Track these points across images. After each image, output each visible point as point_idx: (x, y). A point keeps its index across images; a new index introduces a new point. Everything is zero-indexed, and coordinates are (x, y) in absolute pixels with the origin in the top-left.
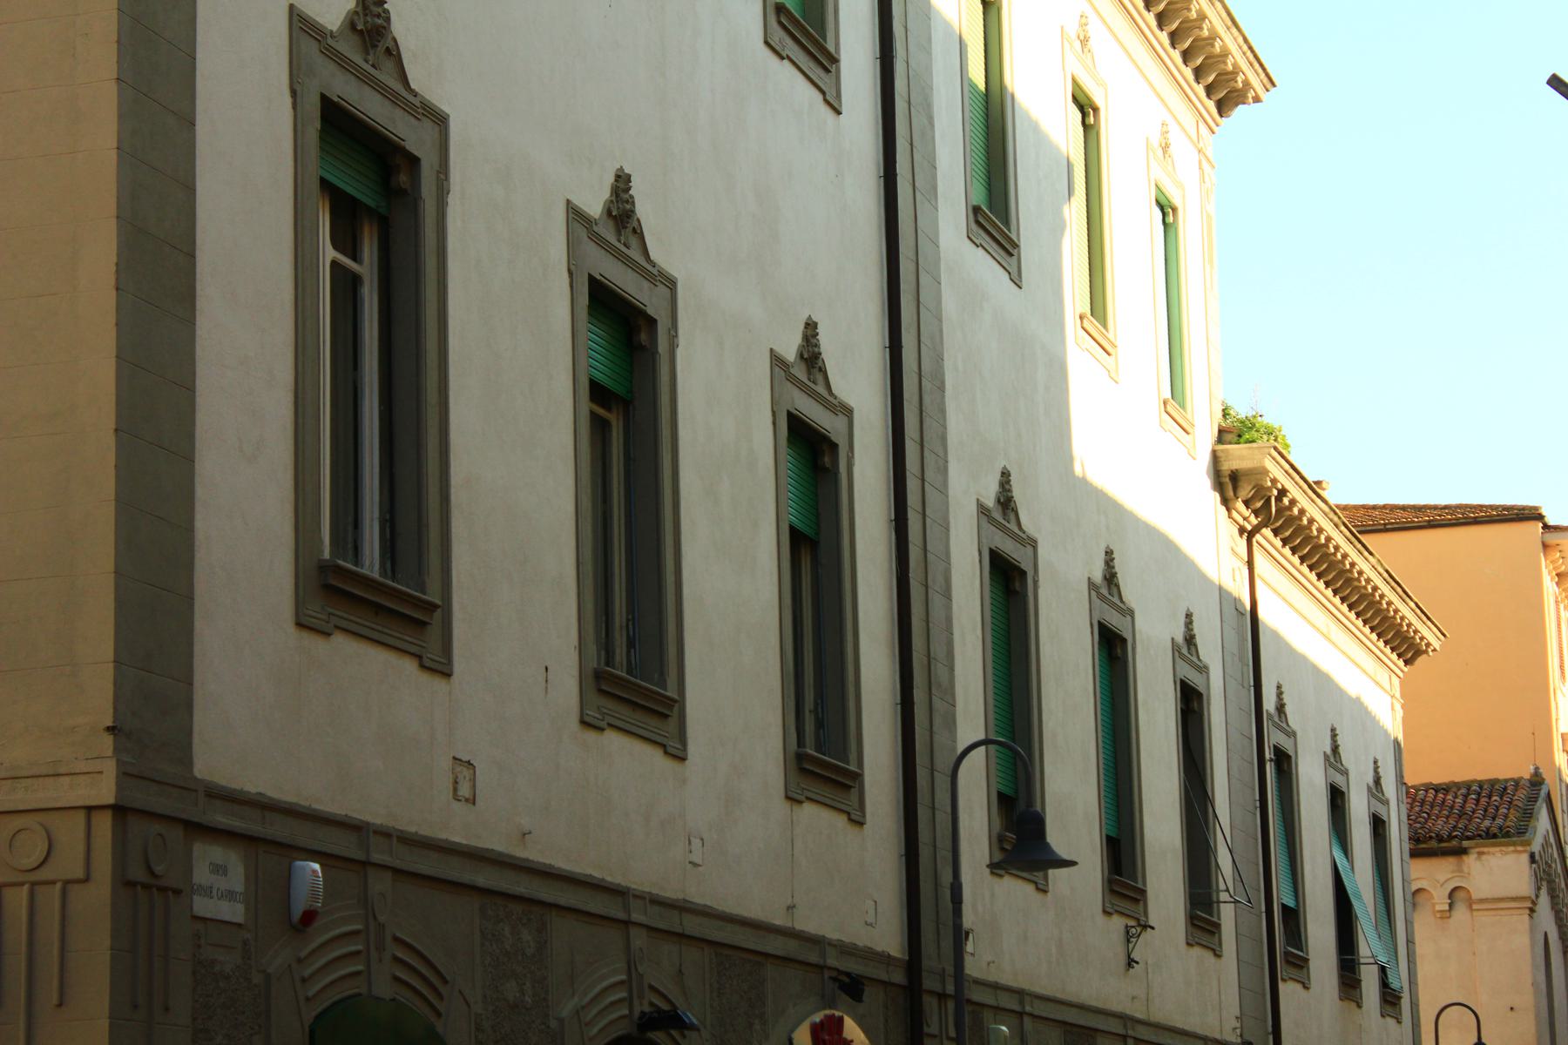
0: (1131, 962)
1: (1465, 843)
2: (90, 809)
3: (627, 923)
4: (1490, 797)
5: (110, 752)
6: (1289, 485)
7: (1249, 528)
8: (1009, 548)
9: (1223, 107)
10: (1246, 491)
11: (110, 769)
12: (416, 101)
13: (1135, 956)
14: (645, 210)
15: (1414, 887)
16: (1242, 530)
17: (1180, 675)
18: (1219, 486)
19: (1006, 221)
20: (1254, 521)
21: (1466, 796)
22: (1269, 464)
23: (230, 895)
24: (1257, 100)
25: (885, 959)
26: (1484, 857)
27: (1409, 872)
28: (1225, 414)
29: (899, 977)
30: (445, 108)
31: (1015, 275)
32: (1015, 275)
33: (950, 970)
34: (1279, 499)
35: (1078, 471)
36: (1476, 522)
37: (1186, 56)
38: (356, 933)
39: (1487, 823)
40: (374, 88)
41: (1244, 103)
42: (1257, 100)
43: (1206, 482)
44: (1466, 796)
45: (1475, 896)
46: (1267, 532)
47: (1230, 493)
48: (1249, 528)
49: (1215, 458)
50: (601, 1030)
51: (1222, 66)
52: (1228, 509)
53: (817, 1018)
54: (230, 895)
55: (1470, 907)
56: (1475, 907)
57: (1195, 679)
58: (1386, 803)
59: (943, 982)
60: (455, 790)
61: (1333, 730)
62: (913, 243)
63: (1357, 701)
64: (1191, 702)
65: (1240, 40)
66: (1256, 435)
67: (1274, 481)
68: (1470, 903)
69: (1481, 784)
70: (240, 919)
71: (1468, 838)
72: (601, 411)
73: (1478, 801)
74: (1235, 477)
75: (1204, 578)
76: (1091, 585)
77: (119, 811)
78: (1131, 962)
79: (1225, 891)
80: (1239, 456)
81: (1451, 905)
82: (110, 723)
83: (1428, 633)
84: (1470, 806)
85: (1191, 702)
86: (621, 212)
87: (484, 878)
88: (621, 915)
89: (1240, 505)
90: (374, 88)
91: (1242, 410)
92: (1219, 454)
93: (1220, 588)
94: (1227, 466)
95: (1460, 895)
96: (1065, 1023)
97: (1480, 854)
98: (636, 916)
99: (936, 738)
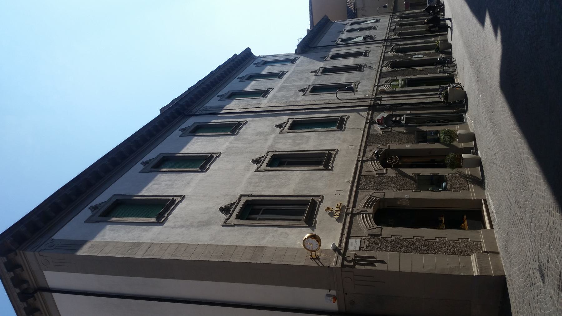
2: (342, 271)
8: (321, 71)
12: (238, 200)
14: (257, 157)
17: (287, 130)
19: (264, 91)
23: (356, 242)
30: (239, 195)
31: (272, 89)
32: (272, 89)
33: (370, 100)
37: (244, 61)
38: (362, 215)
50: (378, 166)
54: (356, 242)
57: (350, 23)
59: (372, 101)
61: (338, 32)
62: (266, 108)
64: (326, 71)
72: (286, 164)
79: (315, 252)
81: (364, 10)
86: (257, 161)
98: (361, 159)
99: (336, 102)
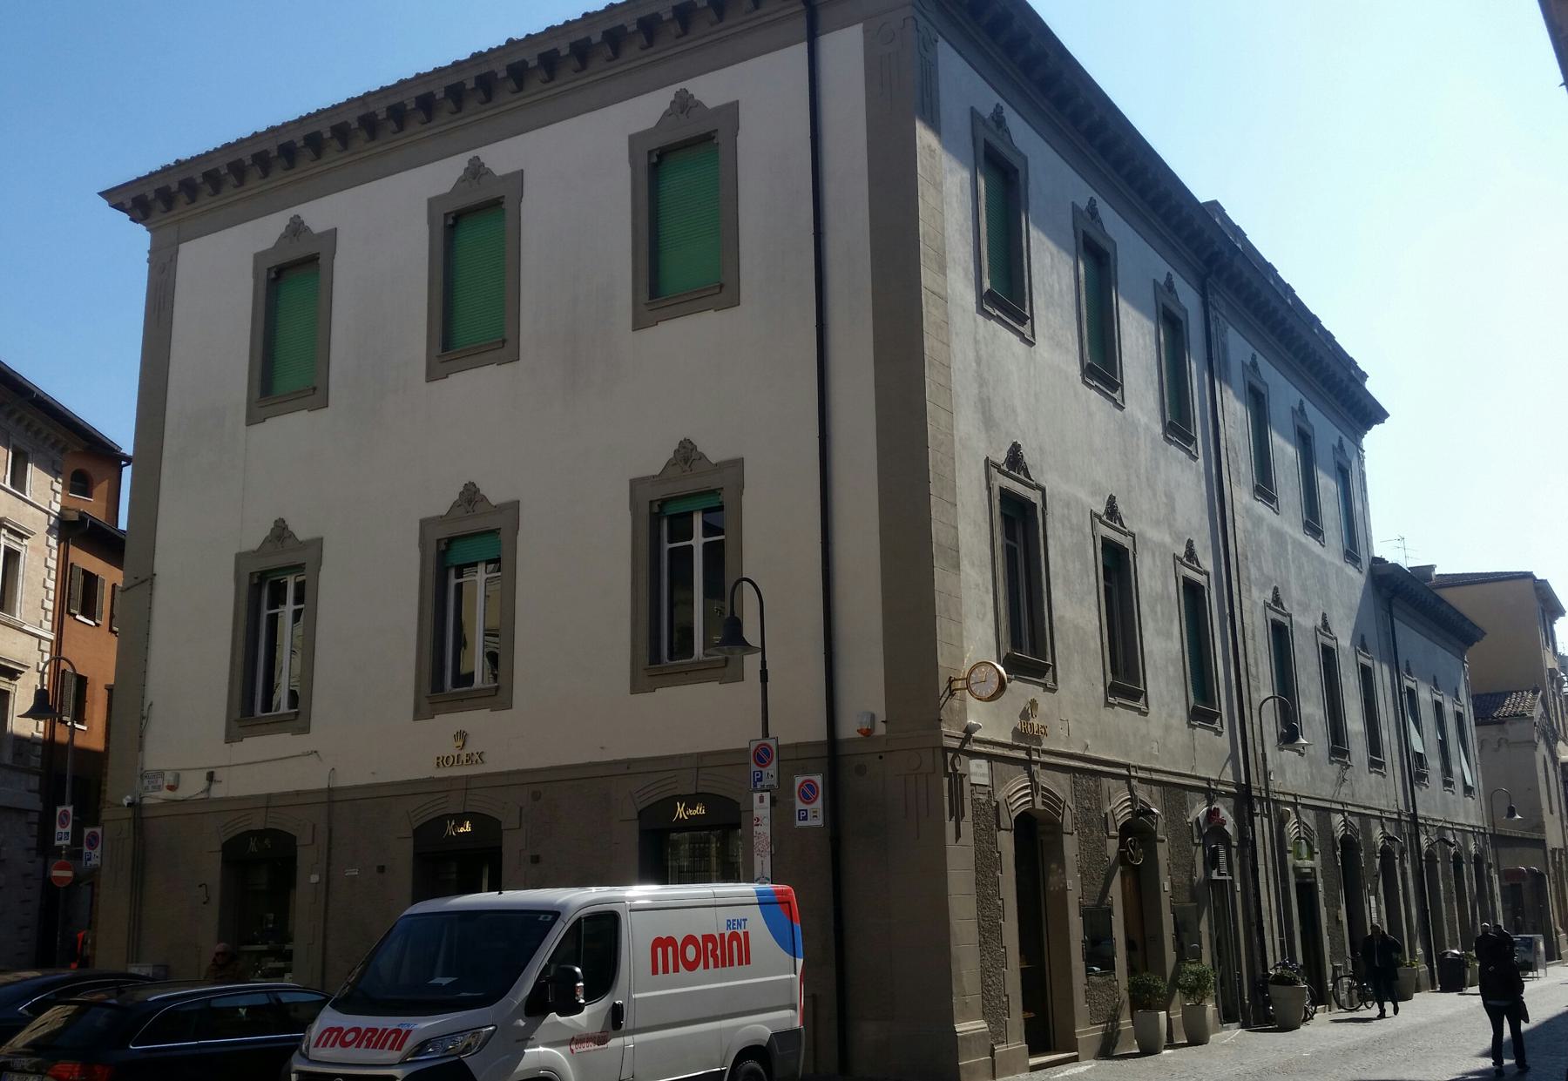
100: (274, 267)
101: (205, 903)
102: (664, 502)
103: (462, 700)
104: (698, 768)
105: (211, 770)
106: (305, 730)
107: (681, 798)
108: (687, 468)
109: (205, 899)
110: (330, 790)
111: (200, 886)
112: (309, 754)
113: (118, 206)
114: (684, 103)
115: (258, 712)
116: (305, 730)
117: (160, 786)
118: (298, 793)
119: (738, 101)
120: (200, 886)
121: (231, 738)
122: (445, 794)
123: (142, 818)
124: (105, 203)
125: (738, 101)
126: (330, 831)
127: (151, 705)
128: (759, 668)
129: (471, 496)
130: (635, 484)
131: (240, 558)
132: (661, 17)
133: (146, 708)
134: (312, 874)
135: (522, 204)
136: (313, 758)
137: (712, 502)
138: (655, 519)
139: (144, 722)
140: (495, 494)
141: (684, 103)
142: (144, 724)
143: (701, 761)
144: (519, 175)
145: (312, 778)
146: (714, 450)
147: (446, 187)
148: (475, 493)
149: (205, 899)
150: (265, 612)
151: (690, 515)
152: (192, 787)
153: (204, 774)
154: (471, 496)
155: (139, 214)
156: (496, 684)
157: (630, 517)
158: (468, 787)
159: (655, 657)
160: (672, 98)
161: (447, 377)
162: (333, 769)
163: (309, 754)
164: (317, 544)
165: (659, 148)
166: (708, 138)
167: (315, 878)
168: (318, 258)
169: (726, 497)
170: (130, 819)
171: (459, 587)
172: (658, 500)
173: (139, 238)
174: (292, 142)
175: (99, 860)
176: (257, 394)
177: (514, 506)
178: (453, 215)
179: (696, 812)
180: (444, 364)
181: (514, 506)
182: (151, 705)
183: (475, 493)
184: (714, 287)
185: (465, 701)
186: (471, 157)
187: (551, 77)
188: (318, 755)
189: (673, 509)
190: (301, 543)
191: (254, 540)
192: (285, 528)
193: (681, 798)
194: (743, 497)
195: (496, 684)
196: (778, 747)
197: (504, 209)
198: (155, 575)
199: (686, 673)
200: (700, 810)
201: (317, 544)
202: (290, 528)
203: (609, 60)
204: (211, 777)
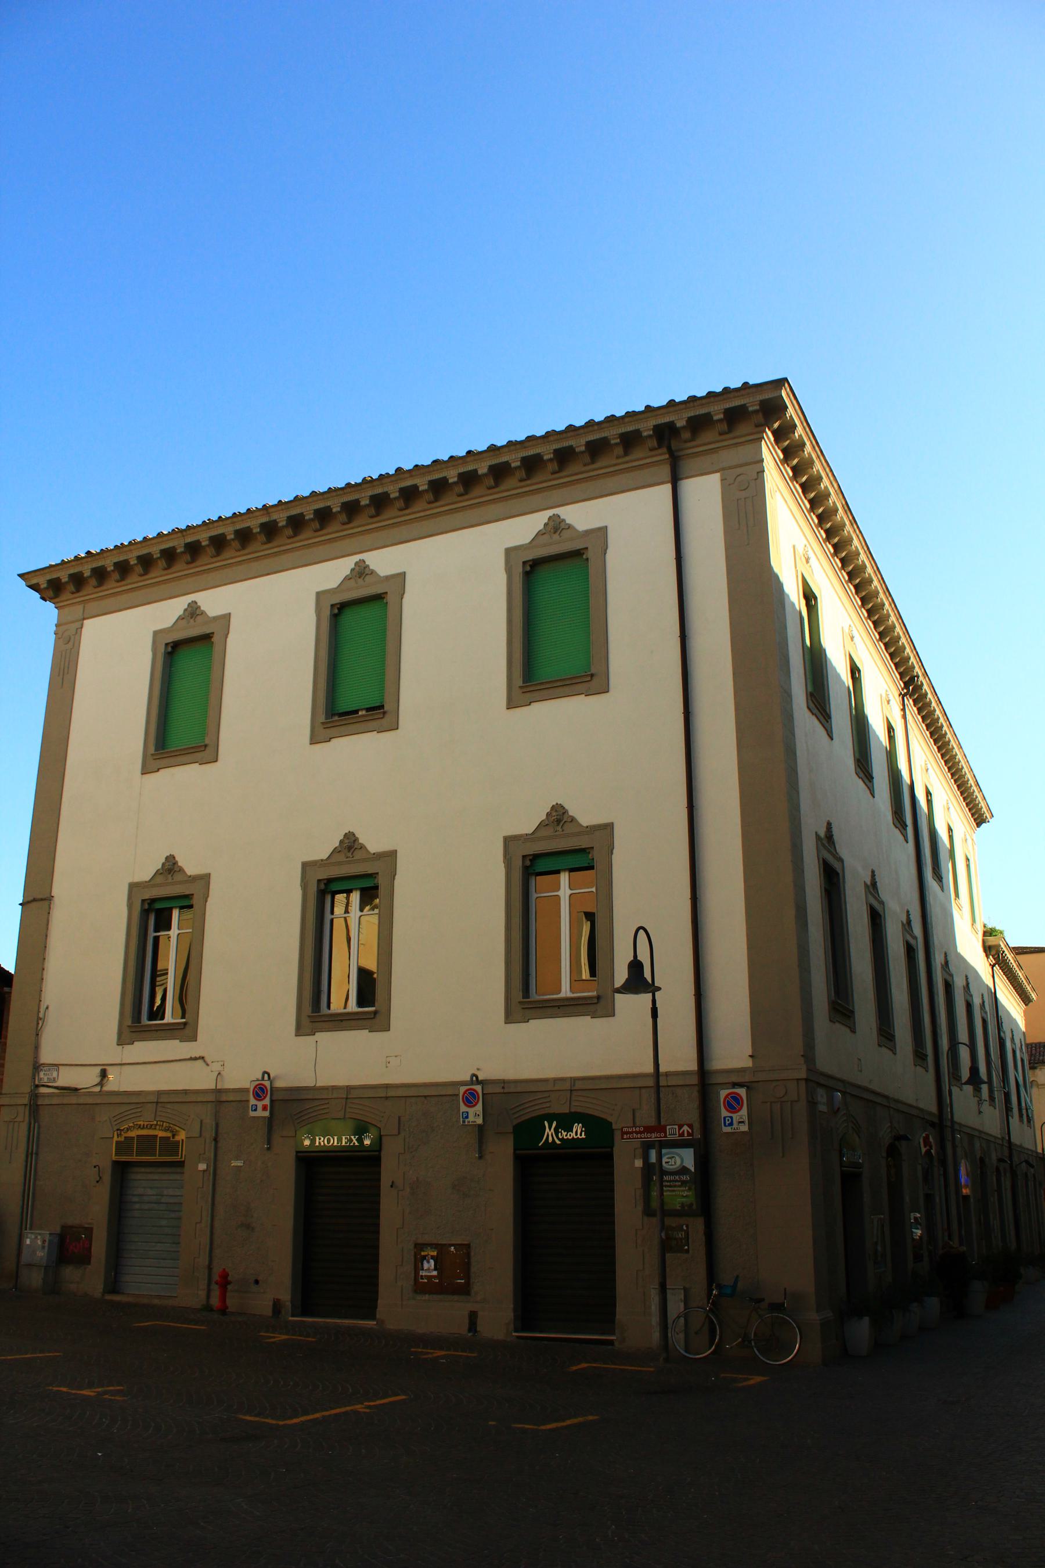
0: (980, 1112)
1: (1036, 1065)
2: (798, 1079)
3: (889, 1107)
4: (1040, 1049)
5: (803, 1062)
6: (1005, 950)
7: (992, 964)
9: (979, 825)
10: (993, 952)
11: (804, 1068)
13: (981, 1110)
15: (1031, 1080)
16: (990, 964)
18: (985, 951)
20: (994, 962)
21: (1031, 1048)
22: (1001, 943)
24: (989, 822)
25: (930, 1113)
26: (1043, 1070)
27: (1030, 1075)
28: (985, 926)
29: (936, 1120)
34: (1002, 954)
35: (958, 951)
36: (1026, 953)
39: (1041, 1058)
40: (176, 755)
41: (985, 822)
42: (989, 822)
43: (981, 949)
44: (1031, 1048)
45: (1039, 1083)
46: (997, 965)
47: (988, 952)
48: (992, 964)
49: (984, 942)
51: (980, 812)
52: (988, 959)
53: (924, 1135)
55: (1038, 1087)
56: (1040, 1087)
58: (986, 1013)
60: (595, 1003)
63: (1015, 1020)
64: (984, 1022)
65: (985, 803)
66: (997, 934)
67: (1002, 948)
68: (1038, 1085)
69: (1036, 1044)
70: (826, 1111)
71: (1036, 1063)
73: (1036, 1050)
74: (990, 948)
75: (984, 983)
76: (964, 987)
77: (806, 1080)
78: (980, 1112)
80: (992, 941)
82: (802, 1054)
83: (1033, 996)
84: (1034, 1052)
85: (984, 1022)
87: (865, 1095)
88: (887, 1104)
89: (991, 957)
90: (176, 755)
91: (990, 926)
92: (985, 940)
93: (987, 985)
94: (987, 944)
95: (1034, 1083)
96: (987, 1140)
97: (1041, 1069)
100: (171, 642)
101: (98, 1182)
102: (153, 901)
103: (342, 1020)
104: (571, 1090)
105: (104, 1067)
106: (194, 1038)
107: (550, 1118)
108: (559, 828)
109: (98, 1179)
110: (218, 1091)
111: (95, 1167)
112: (196, 1059)
113: (34, 587)
114: (361, 571)
115: (145, 1021)
116: (194, 1038)
117: (54, 1078)
118: (186, 1092)
119: (230, 614)
120: (95, 1167)
121: (121, 1042)
122: (142, 1105)
123: (37, 1105)
124: (22, 583)
125: (230, 614)
126: (217, 1125)
127: (47, 1008)
128: (651, 1006)
129: (171, 867)
130: (509, 841)
131: (307, 867)
132: (153, 556)
133: (42, 1010)
134: (199, 1162)
135: (404, 600)
136: (200, 1062)
137: (367, 883)
138: (145, 913)
139: (41, 1022)
140: (191, 867)
141: (361, 571)
142: (40, 1025)
143: (574, 1086)
144: (227, 617)
145: (200, 1079)
146: (374, 843)
147: (333, 583)
148: (564, 813)
149: (98, 1179)
150: (152, 934)
151: (170, 909)
152: (86, 1079)
153: (98, 1070)
154: (171, 867)
155: (51, 593)
156: (184, 1020)
157: (504, 869)
158: (159, 1101)
159: (137, 1017)
160: (353, 566)
161: (530, 705)
162: (219, 1073)
163: (196, 1059)
164: (205, 879)
165: (173, 642)
166: (379, 598)
167: (202, 1166)
168: (212, 637)
169: (381, 881)
170: (25, 1105)
171: (156, 940)
172: (324, 879)
173: (49, 612)
174: (198, 542)
175: (676, 1137)
176: (152, 749)
177: (392, 855)
178: (531, 563)
179: (573, 1134)
180: (327, 729)
181: (392, 855)
182: (47, 1008)
183: (355, 841)
184: (201, 746)
185: (344, 1022)
186: (358, 560)
187: (193, 560)
188: (205, 1061)
189: (158, 906)
190: (190, 876)
191: (145, 874)
192: (175, 863)
193: (550, 1118)
194: (613, 856)
195: (184, 1020)
196: (271, 1088)
197: (213, 643)
198: (53, 897)
199: (559, 1007)
200: (578, 1131)
201: (205, 879)
202: (180, 864)
203: (343, 524)
204: (104, 1074)
